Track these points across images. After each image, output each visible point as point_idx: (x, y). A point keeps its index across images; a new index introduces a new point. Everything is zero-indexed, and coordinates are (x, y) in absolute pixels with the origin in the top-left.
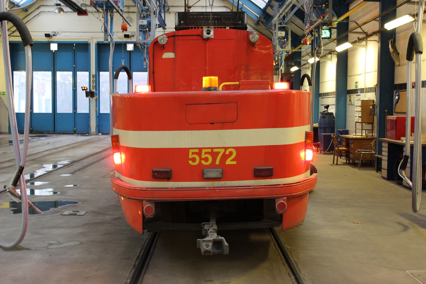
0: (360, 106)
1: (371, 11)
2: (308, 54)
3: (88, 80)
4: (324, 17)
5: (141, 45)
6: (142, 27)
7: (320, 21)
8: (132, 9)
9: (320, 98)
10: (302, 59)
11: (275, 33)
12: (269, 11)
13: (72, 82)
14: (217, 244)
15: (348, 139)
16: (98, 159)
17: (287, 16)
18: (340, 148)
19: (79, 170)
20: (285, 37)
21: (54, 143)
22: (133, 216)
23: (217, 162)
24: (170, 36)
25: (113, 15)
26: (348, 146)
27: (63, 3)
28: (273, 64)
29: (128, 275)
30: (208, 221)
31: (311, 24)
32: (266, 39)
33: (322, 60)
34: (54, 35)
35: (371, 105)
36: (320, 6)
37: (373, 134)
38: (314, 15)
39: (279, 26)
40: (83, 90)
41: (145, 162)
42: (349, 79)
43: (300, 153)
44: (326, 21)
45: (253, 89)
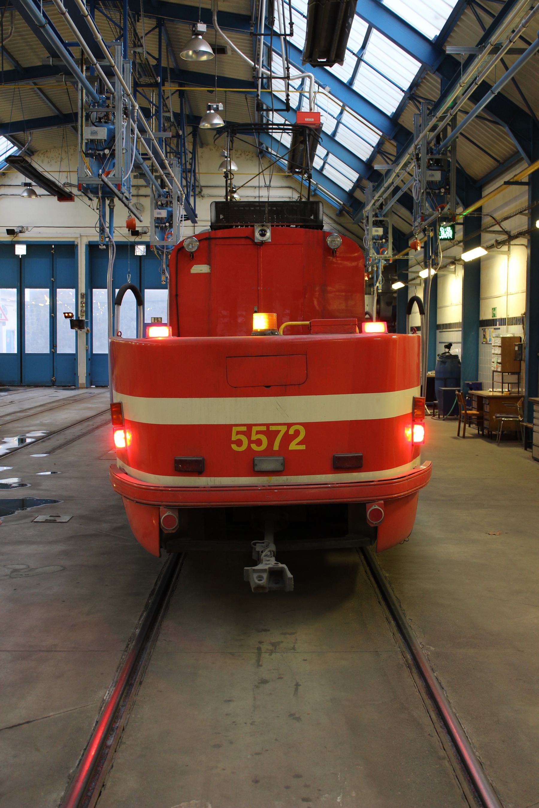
0: (499, 346)
1: (515, 198)
2: (419, 264)
3: (74, 300)
4: (442, 210)
5: (157, 248)
6: (159, 221)
7: (437, 214)
8: (143, 191)
9: (438, 331)
10: (410, 270)
11: (368, 230)
12: (358, 194)
13: (48, 303)
14: (275, 575)
15: (481, 398)
16: (91, 428)
17: (386, 203)
18: (468, 412)
19: (60, 447)
20: (382, 236)
21: (20, 401)
22: (144, 529)
23: (276, 447)
24: (202, 238)
25: (114, 206)
26: (480, 408)
27: (35, 182)
28: (364, 277)
29: (136, 622)
30: (261, 537)
31: (423, 219)
32: (355, 242)
33: (440, 273)
34: (21, 232)
35: (516, 345)
36: (437, 191)
37: (520, 390)
38: (427, 205)
39: (374, 219)
40: (66, 317)
41: (162, 445)
42: (482, 303)
43: (404, 430)
44: (447, 214)
45: (332, 332)
